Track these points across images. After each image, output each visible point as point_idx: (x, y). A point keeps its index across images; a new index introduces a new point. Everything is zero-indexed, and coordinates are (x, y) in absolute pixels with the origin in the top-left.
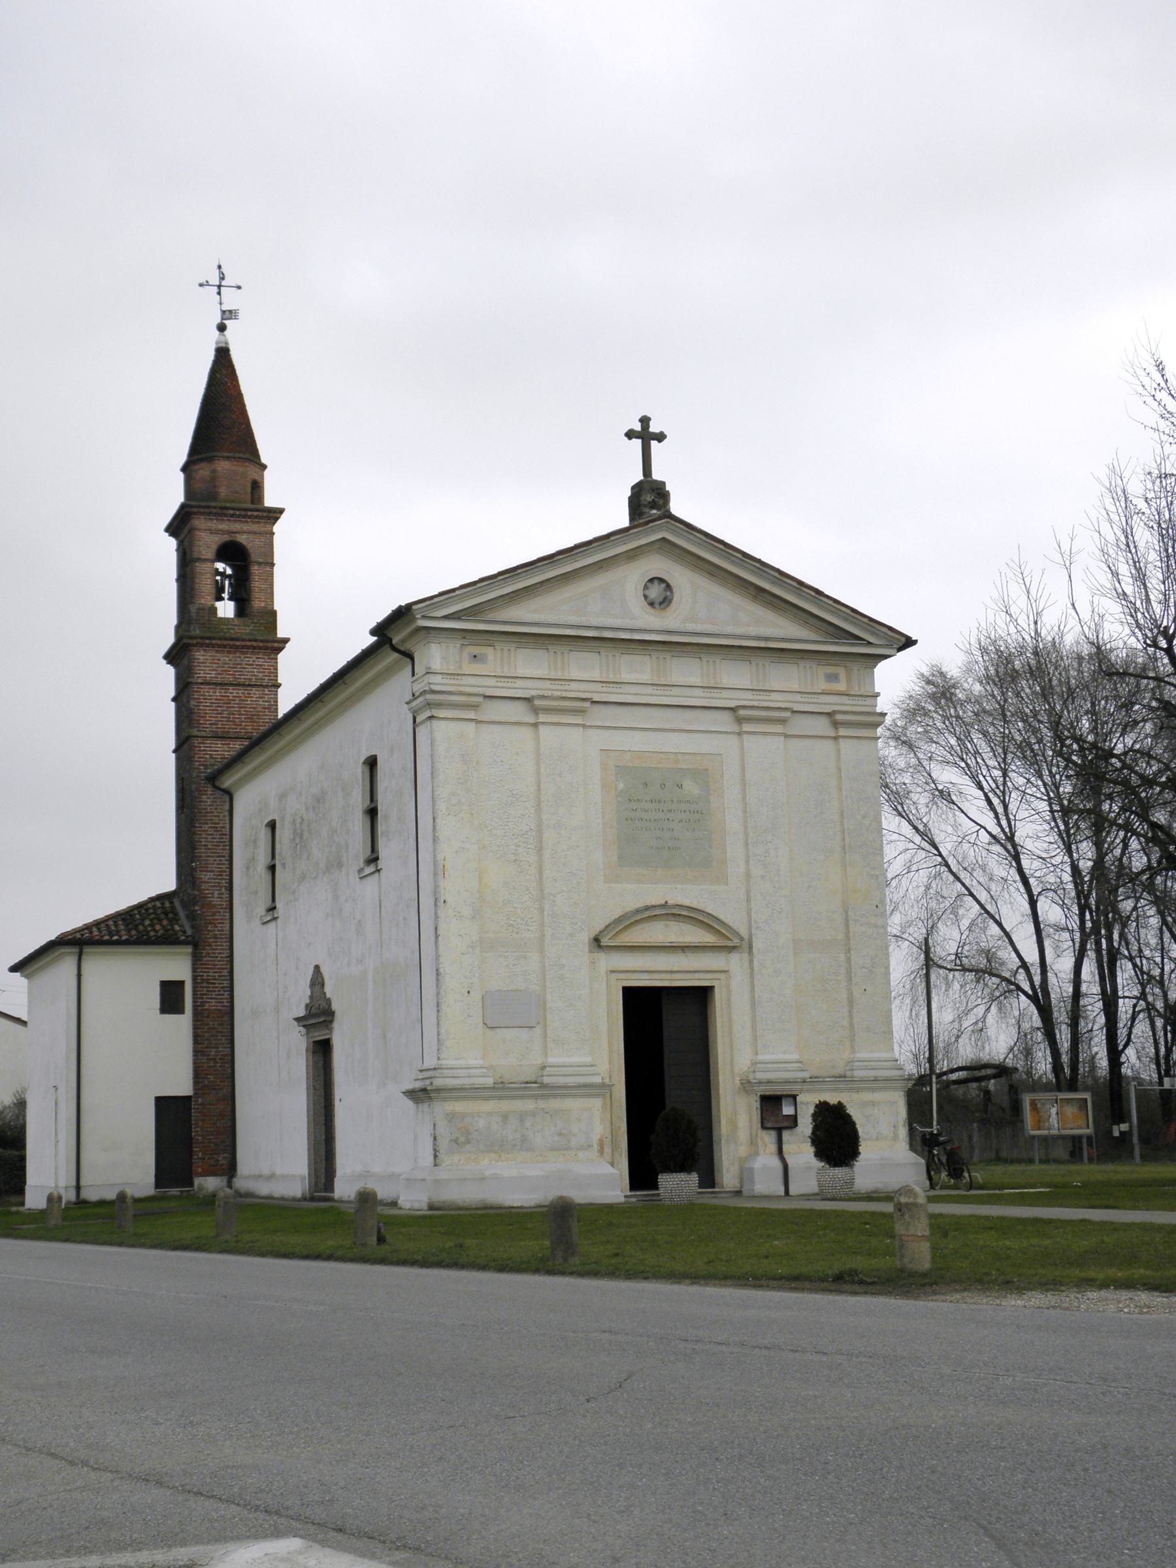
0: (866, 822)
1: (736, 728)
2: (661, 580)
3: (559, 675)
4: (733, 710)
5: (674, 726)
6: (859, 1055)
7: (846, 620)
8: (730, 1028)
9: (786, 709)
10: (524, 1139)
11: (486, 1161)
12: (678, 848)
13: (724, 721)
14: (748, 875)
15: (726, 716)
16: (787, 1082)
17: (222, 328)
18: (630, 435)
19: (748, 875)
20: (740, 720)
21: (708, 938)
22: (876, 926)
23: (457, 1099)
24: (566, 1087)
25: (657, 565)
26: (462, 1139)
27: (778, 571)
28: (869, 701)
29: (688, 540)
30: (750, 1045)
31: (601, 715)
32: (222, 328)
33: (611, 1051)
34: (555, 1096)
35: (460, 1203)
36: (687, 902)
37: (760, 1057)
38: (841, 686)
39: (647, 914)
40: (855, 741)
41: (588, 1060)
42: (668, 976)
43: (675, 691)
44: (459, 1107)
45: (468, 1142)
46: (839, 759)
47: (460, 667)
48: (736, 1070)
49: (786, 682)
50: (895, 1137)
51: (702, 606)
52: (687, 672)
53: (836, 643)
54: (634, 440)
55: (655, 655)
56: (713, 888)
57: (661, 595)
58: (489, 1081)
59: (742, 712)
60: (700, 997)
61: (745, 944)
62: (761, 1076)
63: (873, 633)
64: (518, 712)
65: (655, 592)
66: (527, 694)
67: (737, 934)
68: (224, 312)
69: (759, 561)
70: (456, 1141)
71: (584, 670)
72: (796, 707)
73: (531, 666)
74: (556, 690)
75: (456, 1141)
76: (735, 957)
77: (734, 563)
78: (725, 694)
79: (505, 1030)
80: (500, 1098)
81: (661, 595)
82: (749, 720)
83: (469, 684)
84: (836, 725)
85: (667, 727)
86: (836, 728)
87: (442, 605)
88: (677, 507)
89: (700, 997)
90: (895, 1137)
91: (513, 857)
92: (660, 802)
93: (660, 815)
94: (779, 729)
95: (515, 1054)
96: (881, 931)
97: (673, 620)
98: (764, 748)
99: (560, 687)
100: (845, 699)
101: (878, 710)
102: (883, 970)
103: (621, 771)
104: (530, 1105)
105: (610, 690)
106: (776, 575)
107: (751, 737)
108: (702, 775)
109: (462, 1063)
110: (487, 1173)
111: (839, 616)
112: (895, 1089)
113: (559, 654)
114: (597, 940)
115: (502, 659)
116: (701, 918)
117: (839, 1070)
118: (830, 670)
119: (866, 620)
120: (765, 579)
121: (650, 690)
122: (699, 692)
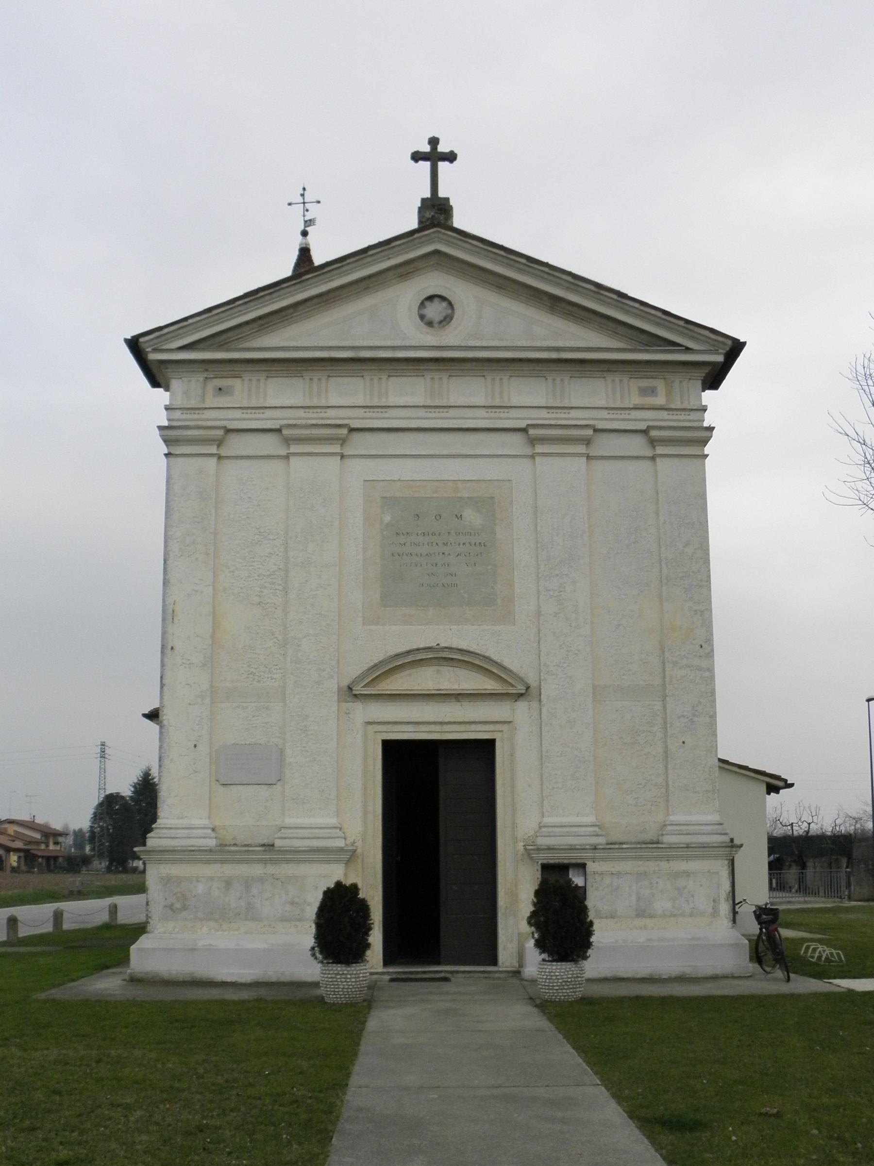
0: (689, 550)
1: (528, 451)
2: (443, 298)
3: (315, 402)
4: (524, 430)
5: (454, 452)
6: (672, 818)
7: (658, 324)
8: (513, 787)
9: (586, 426)
10: (250, 907)
11: (205, 930)
12: (455, 585)
13: (515, 444)
14: (539, 613)
15: (517, 439)
16: (572, 848)
17: (305, 234)
18: (417, 157)
19: (539, 613)
20: (533, 442)
21: (490, 685)
22: (700, 669)
23: (174, 861)
24: (296, 851)
25: (435, 281)
26: (178, 905)
27: (570, 274)
28: (694, 416)
29: (465, 250)
30: (537, 808)
31: (361, 444)
32: (305, 234)
33: (365, 813)
34: (288, 861)
35: (166, 976)
36: (463, 645)
37: (547, 820)
38: (660, 400)
39: (410, 658)
40: (676, 460)
41: (333, 821)
42: (438, 728)
43: (453, 413)
44: (175, 870)
45: (184, 908)
46: (656, 483)
47: (203, 401)
48: (520, 834)
49: (589, 398)
50: (715, 913)
51: (485, 319)
52: (468, 393)
53: (647, 351)
54: (421, 162)
55: (428, 375)
56: (498, 628)
57: (437, 310)
58: (212, 843)
59: (532, 432)
60: (484, 750)
61: (533, 690)
62: (543, 841)
63: (692, 338)
64: (269, 444)
65: (434, 311)
66: (276, 425)
67: (521, 680)
68: (306, 222)
69: (547, 265)
70: (171, 907)
71: (345, 395)
72: (600, 425)
73: (283, 396)
74: (313, 417)
75: (171, 907)
76: (522, 706)
77: (519, 270)
78: (513, 413)
79: (239, 787)
80: (223, 862)
81: (437, 310)
82: (543, 440)
83: (211, 417)
84: (653, 442)
85: (445, 452)
86: (654, 447)
87: (176, 336)
88: (459, 221)
89: (484, 750)
90: (715, 913)
91: (257, 600)
92: (433, 534)
93: (435, 550)
94: (581, 449)
95: (247, 814)
96: (707, 674)
97: (455, 337)
98: (562, 471)
99: (315, 415)
100: (664, 415)
101: (706, 424)
102: (707, 719)
103: (388, 502)
104: (257, 870)
105: (374, 415)
106: (569, 279)
107: (546, 460)
108: (486, 504)
109: (185, 822)
110: (201, 943)
111: (648, 321)
112: (716, 857)
113: (315, 380)
114: (350, 688)
115: (250, 390)
116: (477, 662)
117: (649, 836)
118: (645, 383)
119: (682, 323)
120: (558, 285)
121: (421, 413)
122: (482, 413)
